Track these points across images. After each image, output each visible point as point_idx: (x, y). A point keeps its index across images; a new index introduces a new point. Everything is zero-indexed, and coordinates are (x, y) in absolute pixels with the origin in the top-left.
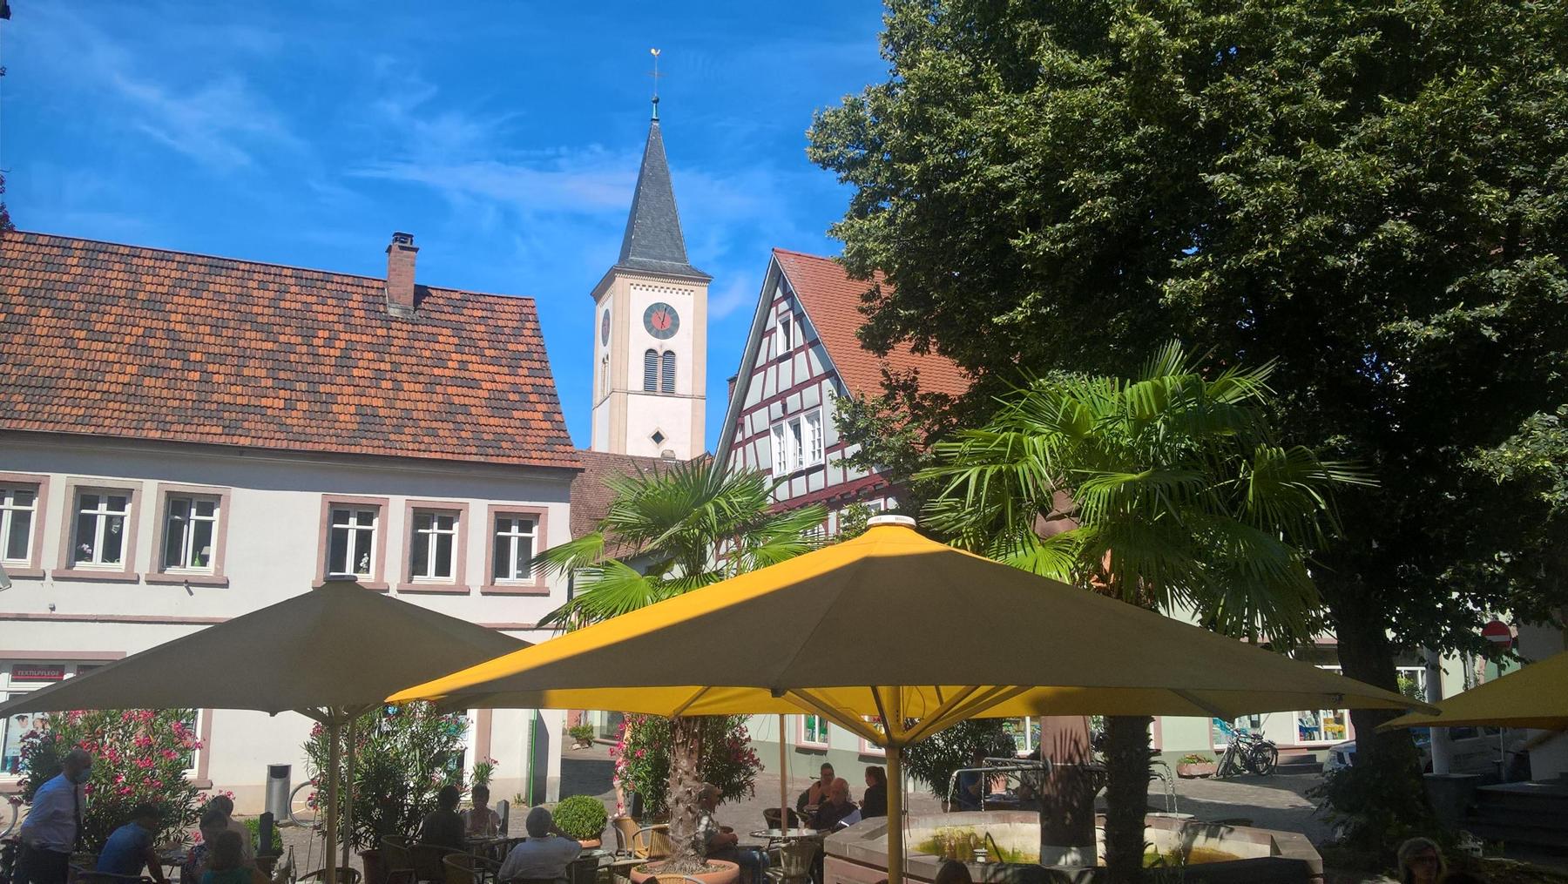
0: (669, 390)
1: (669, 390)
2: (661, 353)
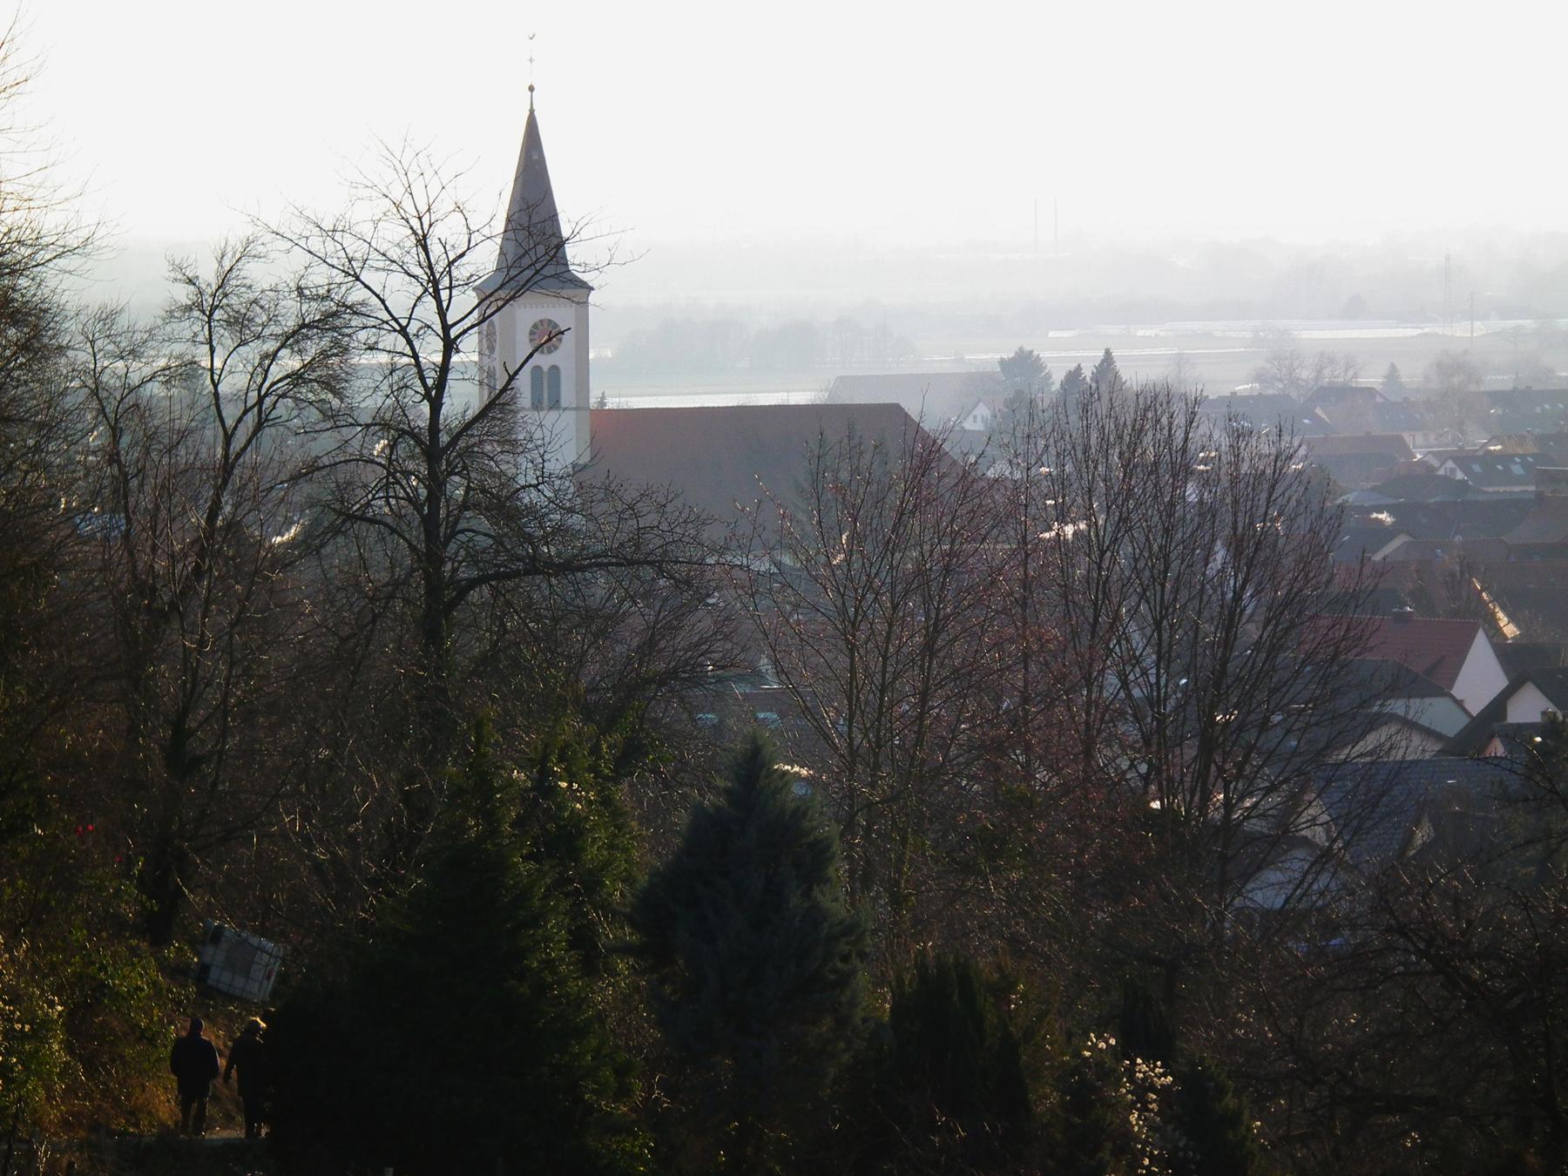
0: (555, 404)
1: (555, 404)
2: (545, 369)
